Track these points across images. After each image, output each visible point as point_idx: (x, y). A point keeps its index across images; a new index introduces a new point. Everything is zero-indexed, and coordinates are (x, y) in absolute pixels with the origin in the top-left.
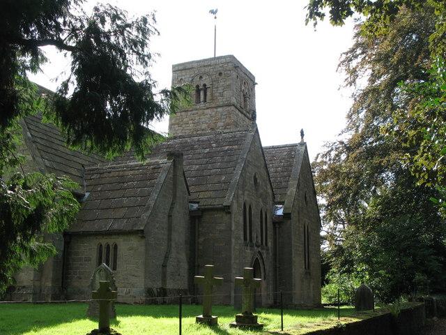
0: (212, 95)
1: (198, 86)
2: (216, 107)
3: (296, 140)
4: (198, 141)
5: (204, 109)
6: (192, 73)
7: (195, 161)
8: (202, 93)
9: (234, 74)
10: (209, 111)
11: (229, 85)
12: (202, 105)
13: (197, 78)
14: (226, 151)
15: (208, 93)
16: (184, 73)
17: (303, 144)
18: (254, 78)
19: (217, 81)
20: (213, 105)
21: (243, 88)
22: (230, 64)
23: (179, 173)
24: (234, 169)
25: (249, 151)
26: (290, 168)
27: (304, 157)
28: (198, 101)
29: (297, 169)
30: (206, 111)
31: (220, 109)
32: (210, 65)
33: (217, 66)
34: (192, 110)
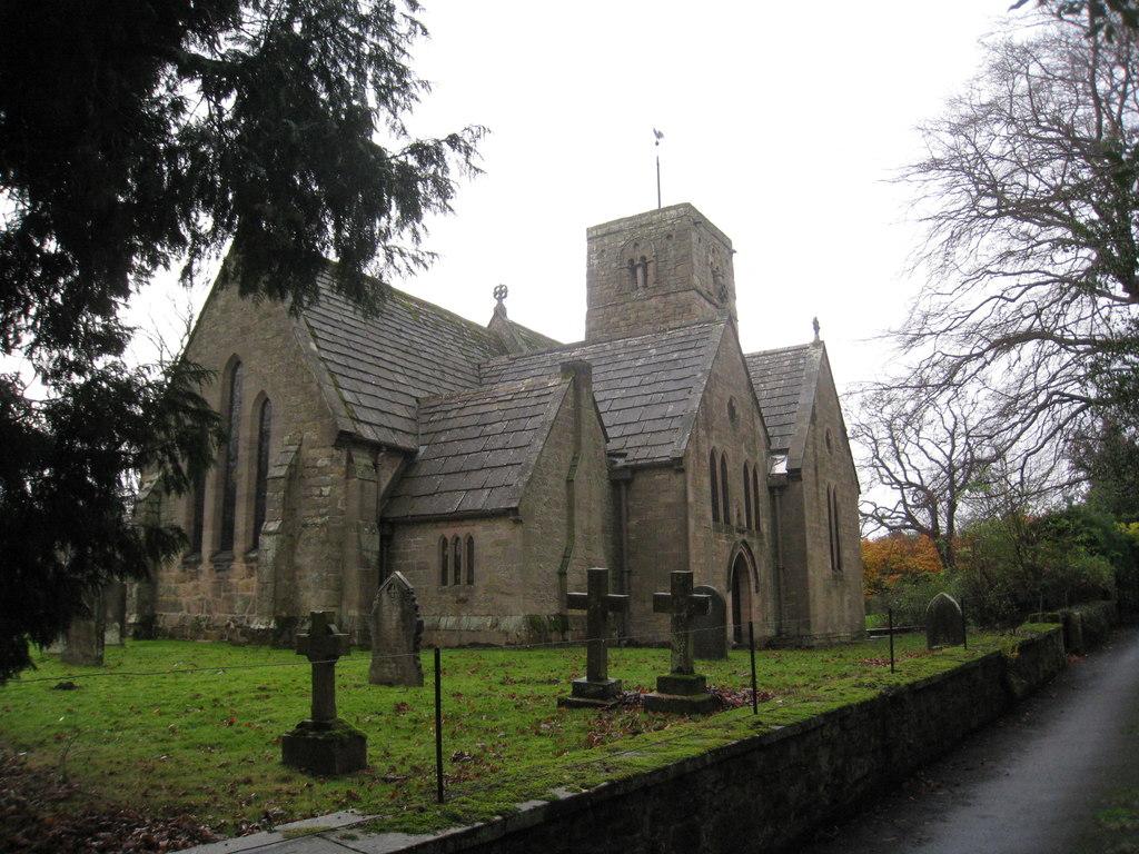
1: (632, 261)
3: (807, 338)
8: (639, 272)
12: (641, 293)
15: (650, 272)
17: (819, 344)
21: (711, 259)
23: (586, 402)
29: (806, 398)
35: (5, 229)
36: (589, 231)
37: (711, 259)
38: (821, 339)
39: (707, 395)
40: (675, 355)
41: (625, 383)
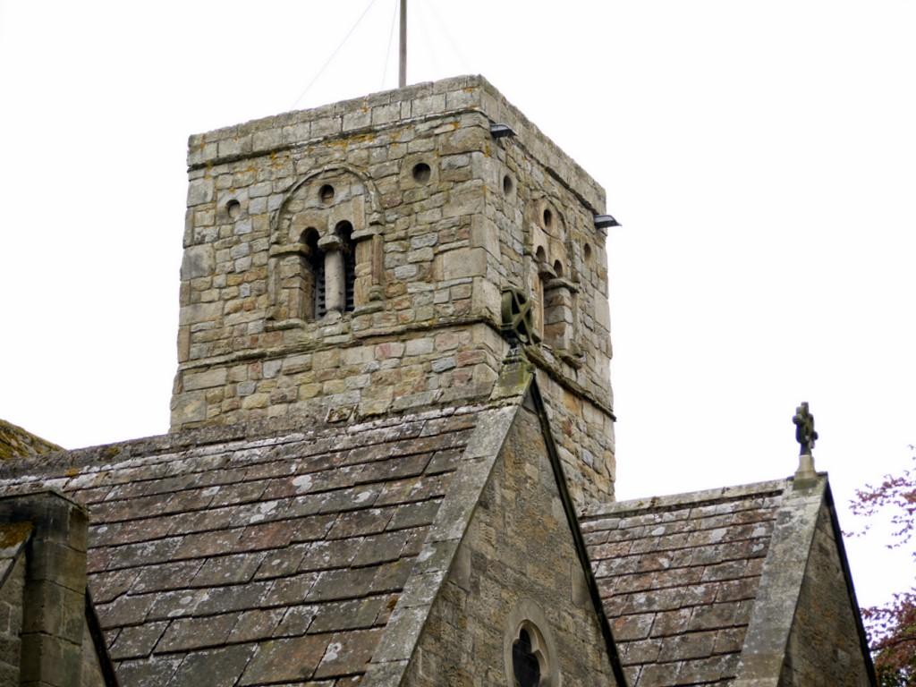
0: (380, 275)
1: (310, 235)
2: (403, 335)
3: (782, 462)
4: (227, 464)
5: (343, 346)
6: (284, 172)
7: (198, 573)
8: (332, 268)
9: (489, 170)
10: (364, 356)
11: (465, 225)
12: (332, 327)
13: (311, 195)
14: (364, 508)
15: (363, 268)
16: (243, 172)
17: (811, 481)
18: (601, 196)
19: (404, 204)
20: (388, 327)
21: (539, 239)
22: (466, 120)
23: (61, 616)
24: (392, 605)
25: (483, 504)
26: (740, 609)
27: (817, 547)
28: (315, 310)
29: (780, 599)
30: (353, 356)
31: (419, 345)
32: (370, 131)
33: (406, 135)
34: (282, 355)
35: (91, 364)
36: (195, 144)
37: (539, 239)
38: (819, 468)
39: (446, 612)
40: (364, 496)
41: (218, 571)
